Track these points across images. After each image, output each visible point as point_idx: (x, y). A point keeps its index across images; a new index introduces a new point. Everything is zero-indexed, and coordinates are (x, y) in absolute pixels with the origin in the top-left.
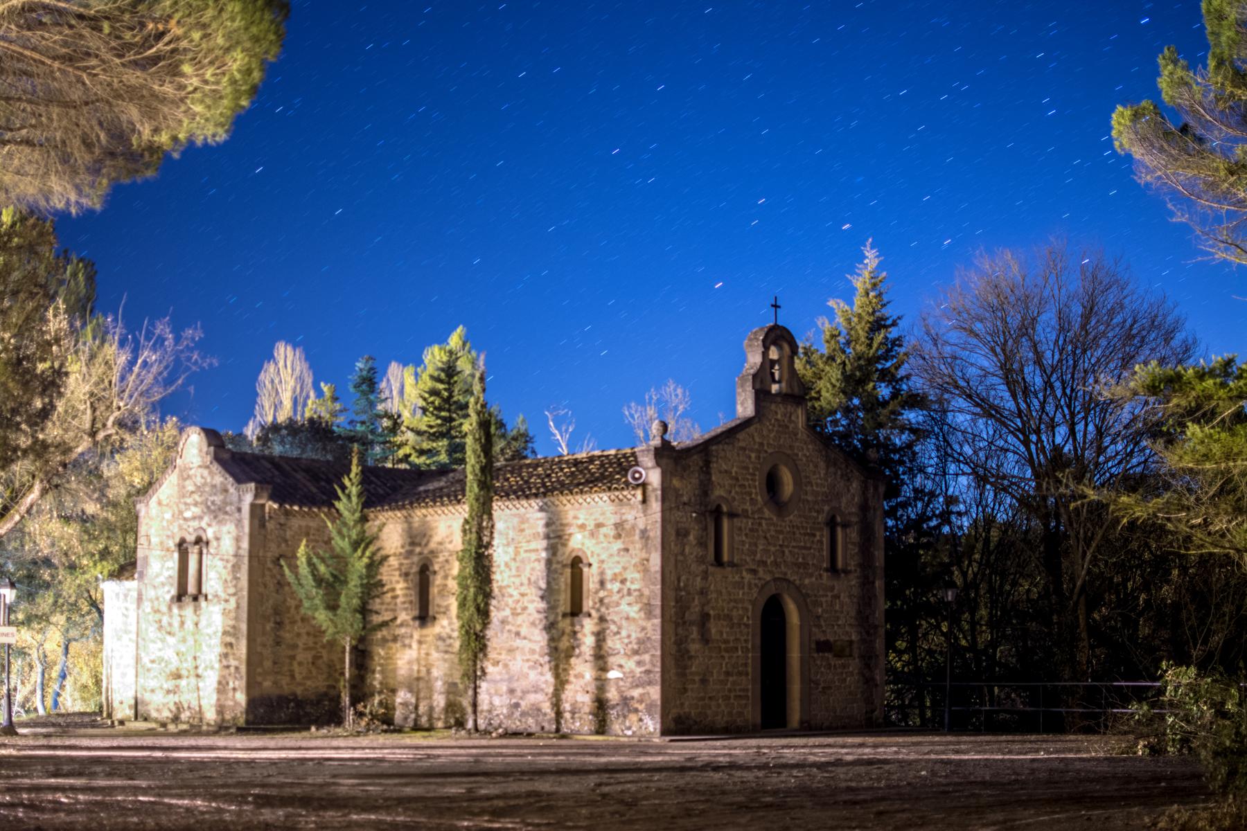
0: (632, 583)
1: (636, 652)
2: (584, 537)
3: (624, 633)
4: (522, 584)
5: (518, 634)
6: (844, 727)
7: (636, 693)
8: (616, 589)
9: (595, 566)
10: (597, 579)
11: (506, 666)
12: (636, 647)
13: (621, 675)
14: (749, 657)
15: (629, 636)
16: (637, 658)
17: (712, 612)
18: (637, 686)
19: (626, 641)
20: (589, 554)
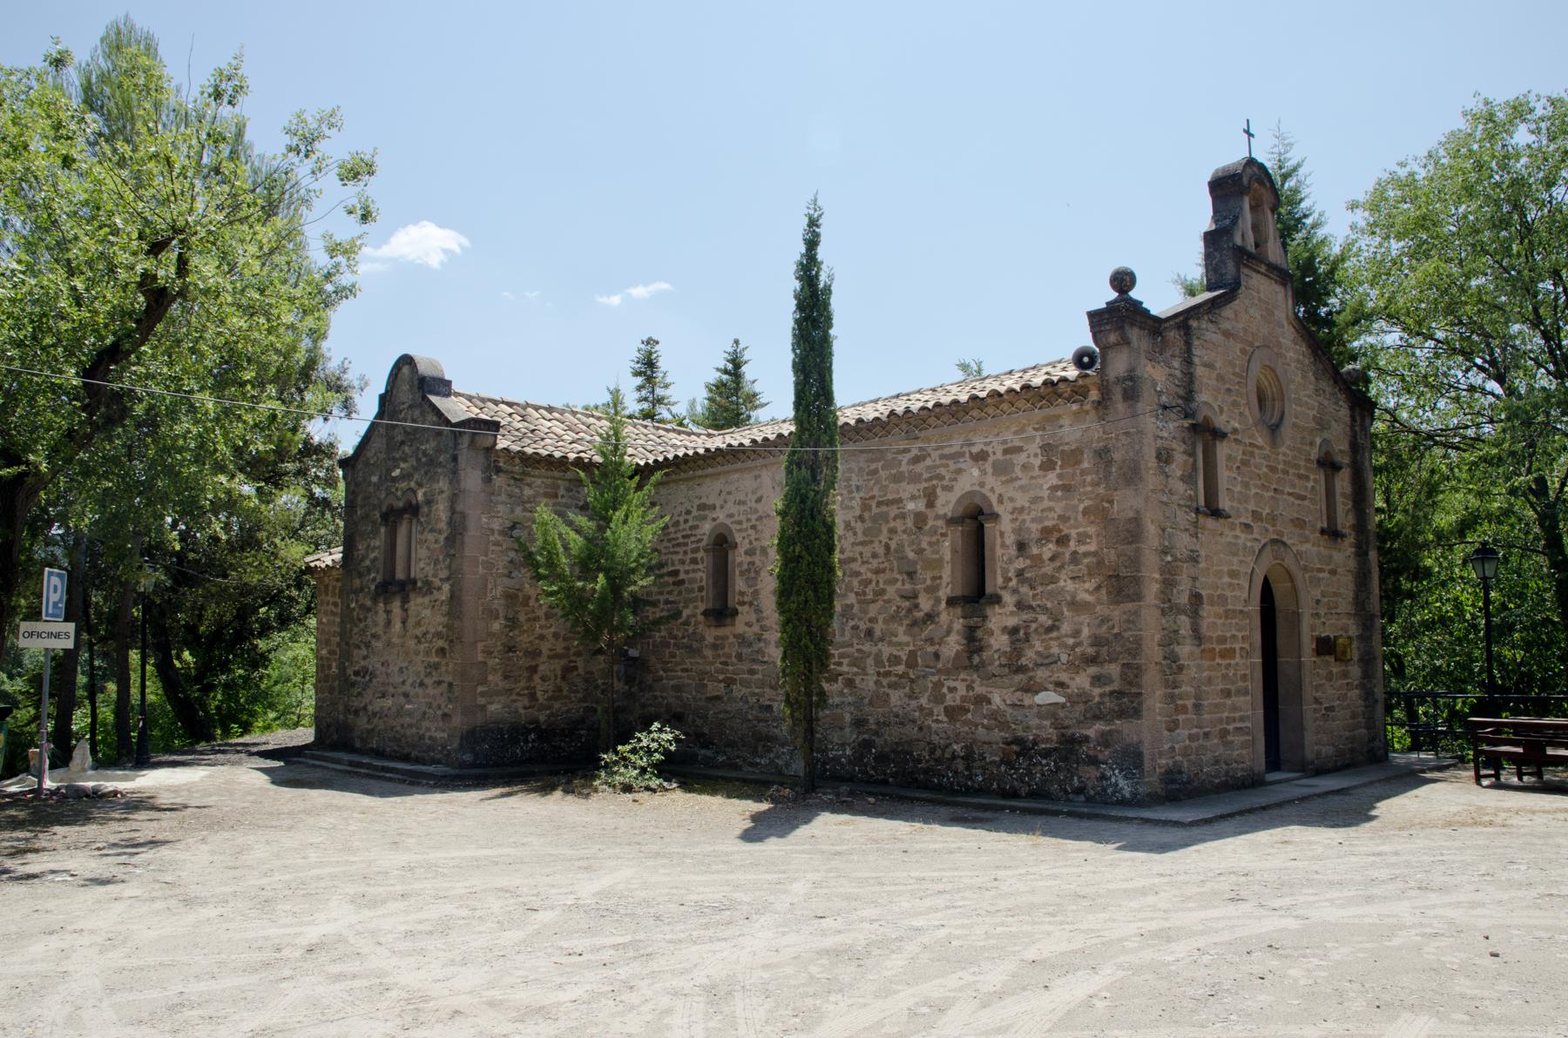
1: (1093, 660)
3: (1066, 628)
5: (869, 633)
7: (1093, 730)
8: (1047, 555)
10: (1010, 539)
12: (1091, 651)
13: (1062, 700)
15: (1076, 633)
16: (1093, 670)
17: (1204, 593)
18: (1096, 717)
19: (1071, 641)
20: (994, 500)
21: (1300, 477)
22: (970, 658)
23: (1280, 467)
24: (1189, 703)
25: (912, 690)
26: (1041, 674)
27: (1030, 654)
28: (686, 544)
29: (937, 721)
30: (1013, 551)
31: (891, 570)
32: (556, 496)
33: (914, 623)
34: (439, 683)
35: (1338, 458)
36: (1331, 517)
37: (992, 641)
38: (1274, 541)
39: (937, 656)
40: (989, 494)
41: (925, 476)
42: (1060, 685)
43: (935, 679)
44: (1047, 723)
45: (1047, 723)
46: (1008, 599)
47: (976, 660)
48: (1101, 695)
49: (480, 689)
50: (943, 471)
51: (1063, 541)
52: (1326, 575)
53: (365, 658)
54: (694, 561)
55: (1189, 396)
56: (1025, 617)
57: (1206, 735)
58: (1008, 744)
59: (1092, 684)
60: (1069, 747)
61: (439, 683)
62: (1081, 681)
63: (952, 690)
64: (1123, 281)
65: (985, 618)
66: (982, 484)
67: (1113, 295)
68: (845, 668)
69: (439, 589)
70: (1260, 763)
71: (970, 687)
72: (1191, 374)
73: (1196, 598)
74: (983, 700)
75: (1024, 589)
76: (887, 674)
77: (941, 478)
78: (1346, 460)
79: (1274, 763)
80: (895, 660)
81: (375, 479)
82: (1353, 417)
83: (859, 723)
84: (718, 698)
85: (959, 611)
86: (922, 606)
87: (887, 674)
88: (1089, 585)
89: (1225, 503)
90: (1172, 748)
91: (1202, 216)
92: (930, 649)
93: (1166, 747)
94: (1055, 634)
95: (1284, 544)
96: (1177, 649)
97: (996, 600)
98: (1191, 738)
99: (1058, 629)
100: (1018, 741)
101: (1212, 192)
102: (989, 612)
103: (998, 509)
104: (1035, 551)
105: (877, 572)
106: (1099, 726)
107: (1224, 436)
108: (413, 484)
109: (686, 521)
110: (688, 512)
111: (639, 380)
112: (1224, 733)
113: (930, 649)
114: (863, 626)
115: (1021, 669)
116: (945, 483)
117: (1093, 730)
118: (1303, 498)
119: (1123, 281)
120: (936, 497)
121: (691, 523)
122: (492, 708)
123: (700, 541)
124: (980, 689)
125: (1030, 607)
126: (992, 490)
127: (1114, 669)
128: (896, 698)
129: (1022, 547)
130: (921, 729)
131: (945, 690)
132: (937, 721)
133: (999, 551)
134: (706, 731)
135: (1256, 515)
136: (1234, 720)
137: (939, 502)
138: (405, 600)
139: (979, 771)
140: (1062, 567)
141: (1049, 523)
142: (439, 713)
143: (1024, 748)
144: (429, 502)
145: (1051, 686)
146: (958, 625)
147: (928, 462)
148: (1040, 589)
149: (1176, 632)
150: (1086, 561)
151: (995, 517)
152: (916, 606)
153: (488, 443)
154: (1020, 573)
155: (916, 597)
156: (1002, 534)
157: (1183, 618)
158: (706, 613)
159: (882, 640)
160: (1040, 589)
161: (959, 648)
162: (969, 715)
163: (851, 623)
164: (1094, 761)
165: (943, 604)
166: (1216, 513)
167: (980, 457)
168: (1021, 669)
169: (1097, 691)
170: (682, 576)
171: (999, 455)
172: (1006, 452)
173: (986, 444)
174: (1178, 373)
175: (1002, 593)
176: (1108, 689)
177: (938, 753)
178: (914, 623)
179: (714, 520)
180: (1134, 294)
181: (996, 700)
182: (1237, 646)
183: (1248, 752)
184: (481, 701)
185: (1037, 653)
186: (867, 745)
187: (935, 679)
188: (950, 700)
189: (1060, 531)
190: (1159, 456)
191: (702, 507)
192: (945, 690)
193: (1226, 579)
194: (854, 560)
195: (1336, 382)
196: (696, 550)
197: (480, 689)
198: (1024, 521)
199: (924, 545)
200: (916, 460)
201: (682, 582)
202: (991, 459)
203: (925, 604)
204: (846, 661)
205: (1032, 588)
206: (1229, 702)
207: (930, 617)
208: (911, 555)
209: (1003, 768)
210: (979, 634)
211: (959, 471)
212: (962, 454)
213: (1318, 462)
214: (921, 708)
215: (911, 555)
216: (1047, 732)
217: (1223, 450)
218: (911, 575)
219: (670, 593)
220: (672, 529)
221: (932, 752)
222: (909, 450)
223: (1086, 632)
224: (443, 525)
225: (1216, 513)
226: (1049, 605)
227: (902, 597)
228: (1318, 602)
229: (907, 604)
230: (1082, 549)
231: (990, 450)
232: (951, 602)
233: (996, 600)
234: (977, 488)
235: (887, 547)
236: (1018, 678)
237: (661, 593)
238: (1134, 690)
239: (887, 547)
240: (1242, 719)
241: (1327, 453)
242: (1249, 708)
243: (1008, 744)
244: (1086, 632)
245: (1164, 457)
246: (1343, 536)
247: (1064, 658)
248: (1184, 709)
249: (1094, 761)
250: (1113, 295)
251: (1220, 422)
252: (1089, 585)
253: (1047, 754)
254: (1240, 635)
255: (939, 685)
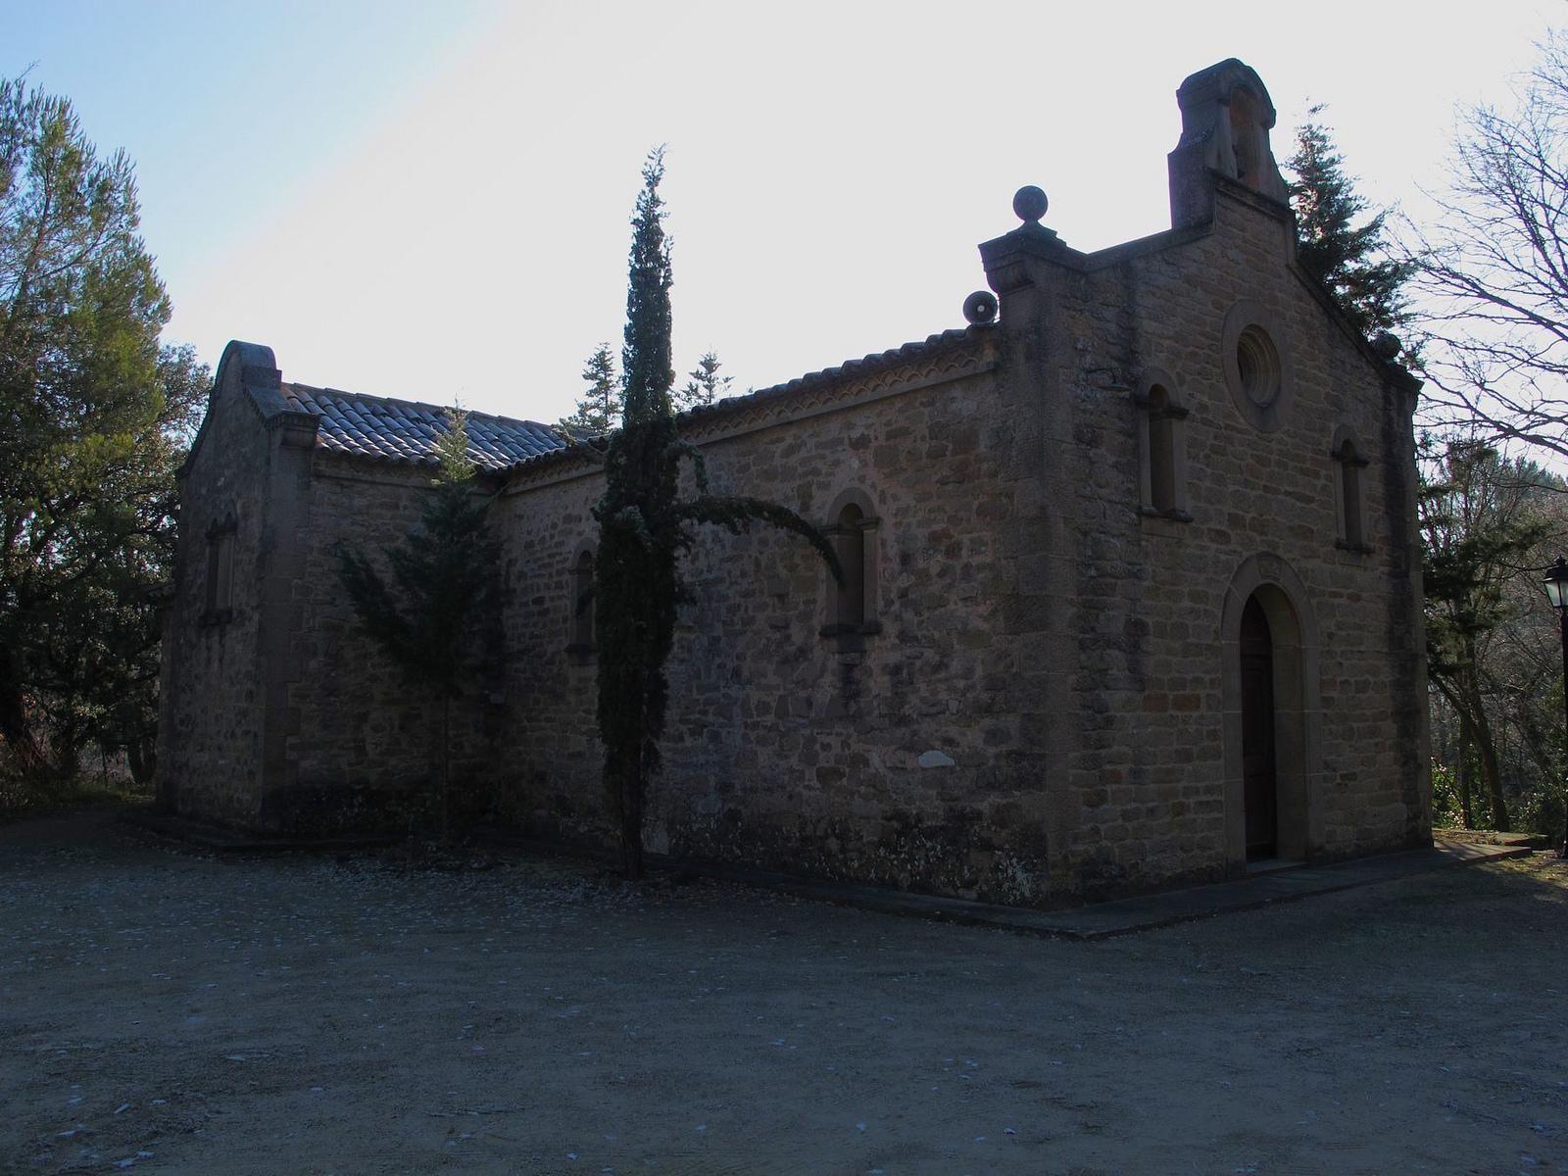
0: (974, 551)
1: (988, 710)
2: (864, 464)
3: (956, 666)
4: (743, 574)
5: (736, 673)
6: (226, 366)
7: (986, 804)
8: (934, 570)
9: (888, 521)
10: (893, 550)
11: (715, 737)
12: (985, 697)
13: (951, 762)
14: (1222, 717)
15: (968, 673)
16: (987, 722)
17: (1149, 621)
18: (991, 787)
19: (961, 684)
20: (875, 499)
21: (1304, 472)
22: (846, 706)
23: (1274, 457)
24: (1124, 769)
25: (781, 747)
26: (926, 728)
27: (914, 700)
28: (551, 565)
29: (809, 788)
30: (896, 565)
31: (762, 592)
32: (397, 507)
33: (785, 661)
34: (247, 733)
35: (1364, 451)
36: (1352, 525)
37: (872, 684)
38: (1261, 556)
39: (809, 703)
40: (868, 491)
41: (800, 470)
42: (949, 742)
43: (807, 732)
44: (933, 793)
45: (933, 793)
46: (891, 628)
47: (853, 707)
48: (997, 757)
49: (290, 740)
50: (818, 464)
51: (953, 551)
52: (1343, 601)
53: (189, 703)
54: (559, 586)
55: (1130, 357)
56: (908, 652)
57: (1151, 811)
58: (889, 819)
59: (986, 742)
60: (960, 821)
61: (247, 733)
62: (973, 737)
63: (826, 747)
64: (1030, 202)
65: (863, 652)
66: (862, 479)
67: (1016, 223)
68: (710, 718)
69: (250, 619)
70: (1239, 851)
71: (845, 744)
72: (1133, 329)
73: (1137, 629)
74: (859, 761)
75: (909, 615)
76: (756, 725)
77: (816, 472)
78: (1377, 453)
79: (1264, 846)
80: (763, 708)
81: (204, 491)
82: (1387, 400)
83: (724, 788)
84: (580, 755)
85: (834, 643)
86: (794, 639)
87: (756, 725)
88: (983, 609)
89: (1185, 503)
90: (1096, 831)
91: (1169, 129)
92: (802, 694)
93: (1086, 828)
94: (942, 675)
95: (1278, 558)
96: (1104, 695)
97: (876, 630)
98: (1126, 816)
99: (947, 666)
100: (899, 816)
101: (1177, 96)
102: (868, 645)
103: (880, 510)
104: (921, 564)
105: (746, 595)
106: (995, 798)
107: (1182, 414)
108: (234, 494)
109: (552, 537)
110: (554, 526)
111: (592, 384)
112: (1180, 809)
113: (802, 694)
114: (730, 665)
115: (902, 721)
116: (821, 479)
117: (986, 804)
118: (1310, 500)
119: (1030, 202)
120: (811, 497)
121: (556, 539)
122: (305, 764)
123: (566, 560)
124: (857, 747)
125: (916, 638)
126: (873, 486)
127: (1012, 722)
128: (764, 756)
129: (906, 559)
130: (790, 797)
131: (817, 747)
132: (809, 788)
133: (880, 567)
134: (568, 796)
135: (1235, 521)
136: (1197, 792)
137: (815, 503)
138: (222, 636)
139: (854, 855)
140: (950, 586)
141: (936, 527)
142: (246, 770)
143: (904, 827)
144: (246, 516)
145: (937, 744)
146: (834, 662)
147: (803, 453)
148: (926, 614)
149: (1104, 672)
150: (981, 576)
151: (877, 522)
152: (788, 638)
153: (308, 437)
154: (903, 594)
155: (787, 627)
156: (884, 544)
157: (1115, 653)
158: (570, 650)
159: (750, 682)
160: (926, 614)
161: (835, 692)
162: (845, 781)
163: (718, 661)
164: (987, 846)
165: (817, 637)
166: (1172, 516)
167: (860, 444)
168: (902, 721)
169: (992, 751)
170: (547, 605)
171: (882, 441)
172: (890, 436)
173: (868, 427)
174: (1113, 327)
175: (883, 620)
176: (1004, 748)
177: (809, 829)
178: (785, 661)
179: (580, 534)
180: (1044, 222)
181: (875, 760)
182: (1202, 693)
183: (1223, 833)
184: (292, 756)
185: (923, 700)
186: (733, 816)
187: (807, 732)
188: (825, 760)
189: (950, 537)
190: (1079, 438)
191: (568, 519)
192: (817, 747)
193: (1186, 603)
194: (721, 580)
195: (1361, 352)
196: (560, 573)
197: (290, 740)
198: (909, 525)
199: (797, 560)
200: (790, 451)
201: (547, 611)
202: (874, 444)
203: (798, 635)
204: (711, 709)
205: (918, 613)
206: (1189, 767)
207: (803, 652)
208: (783, 572)
209: (882, 851)
210: (857, 674)
211: (837, 463)
212: (840, 441)
213: (1333, 454)
214: (792, 771)
215: (783, 572)
216: (930, 806)
217: (1180, 433)
218: (781, 597)
219: (535, 625)
220: (538, 548)
221: (802, 829)
222: (783, 439)
223: (979, 672)
224: (255, 543)
225: (1172, 516)
226: (937, 635)
227: (773, 627)
228: (1331, 636)
229: (778, 635)
230: (976, 560)
231: (872, 434)
232: (826, 634)
233: (876, 630)
234: (856, 484)
235: (757, 564)
236: (902, 732)
237: (526, 626)
238: (1036, 750)
239: (757, 564)
240: (1209, 790)
241: (1347, 444)
242: (1221, 775)
243: (889, 819)
244: (979, 672)
245: (1087, 438)
246: (1369, 552)
247: (954, 706)
248: (1116, 778)
249: (987, 846)
250: (1016, 223)
251: (1179, 395)
252: (983, 609)
253: (931, 834)
254: (1207, 678)
255: (811, 740)
